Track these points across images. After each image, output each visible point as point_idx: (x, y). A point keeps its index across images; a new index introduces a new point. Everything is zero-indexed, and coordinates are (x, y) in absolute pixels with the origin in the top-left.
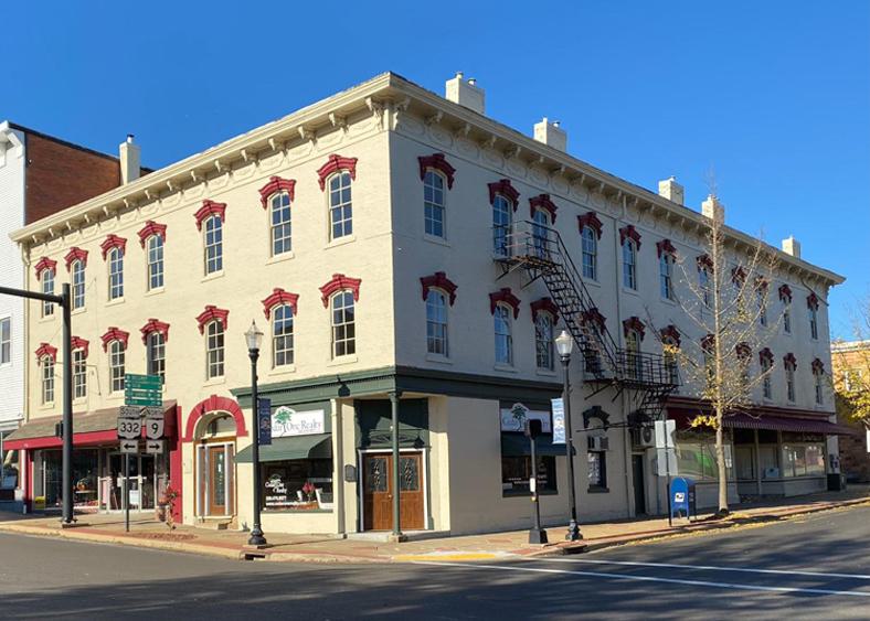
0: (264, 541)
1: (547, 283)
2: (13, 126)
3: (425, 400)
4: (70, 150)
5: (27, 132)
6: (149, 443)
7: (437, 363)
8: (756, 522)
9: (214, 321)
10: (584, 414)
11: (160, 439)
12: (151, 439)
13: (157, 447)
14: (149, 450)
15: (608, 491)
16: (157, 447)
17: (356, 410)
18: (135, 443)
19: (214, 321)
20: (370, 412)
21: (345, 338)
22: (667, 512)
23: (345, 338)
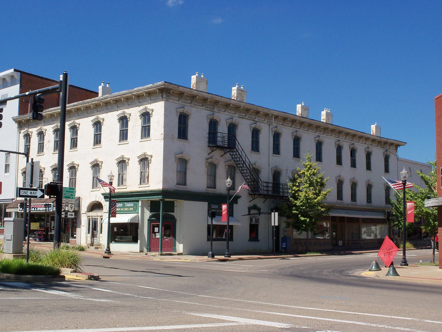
0: (110, 253)
1: (231, 155)
2: (15, 70)
3: (174, 202)
4: (39, 79)
5: (22, 73)
6: (69, 213)
7: (181, 188)
8: (308, 256)
9: (96, 166)
10: (248, 208)
11: (73, 212)
12: (70, 212)
13: (72, 215)
14: (69, 216)
15: (259, 241)
16: (72, 215)
17: (279, 180)
18: (73, 214)
19: (96, 166)
20: (154, 206)
21: (144, 178)
22: (54, 207)
23: (144, 178)
